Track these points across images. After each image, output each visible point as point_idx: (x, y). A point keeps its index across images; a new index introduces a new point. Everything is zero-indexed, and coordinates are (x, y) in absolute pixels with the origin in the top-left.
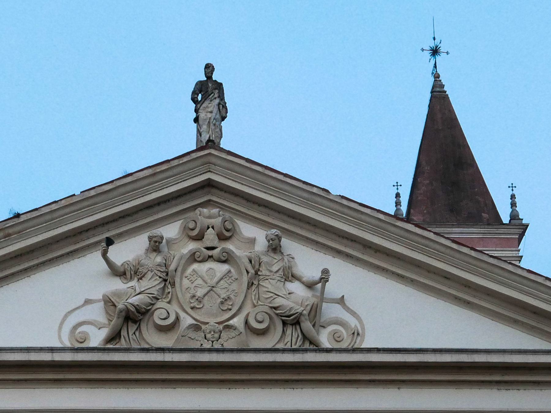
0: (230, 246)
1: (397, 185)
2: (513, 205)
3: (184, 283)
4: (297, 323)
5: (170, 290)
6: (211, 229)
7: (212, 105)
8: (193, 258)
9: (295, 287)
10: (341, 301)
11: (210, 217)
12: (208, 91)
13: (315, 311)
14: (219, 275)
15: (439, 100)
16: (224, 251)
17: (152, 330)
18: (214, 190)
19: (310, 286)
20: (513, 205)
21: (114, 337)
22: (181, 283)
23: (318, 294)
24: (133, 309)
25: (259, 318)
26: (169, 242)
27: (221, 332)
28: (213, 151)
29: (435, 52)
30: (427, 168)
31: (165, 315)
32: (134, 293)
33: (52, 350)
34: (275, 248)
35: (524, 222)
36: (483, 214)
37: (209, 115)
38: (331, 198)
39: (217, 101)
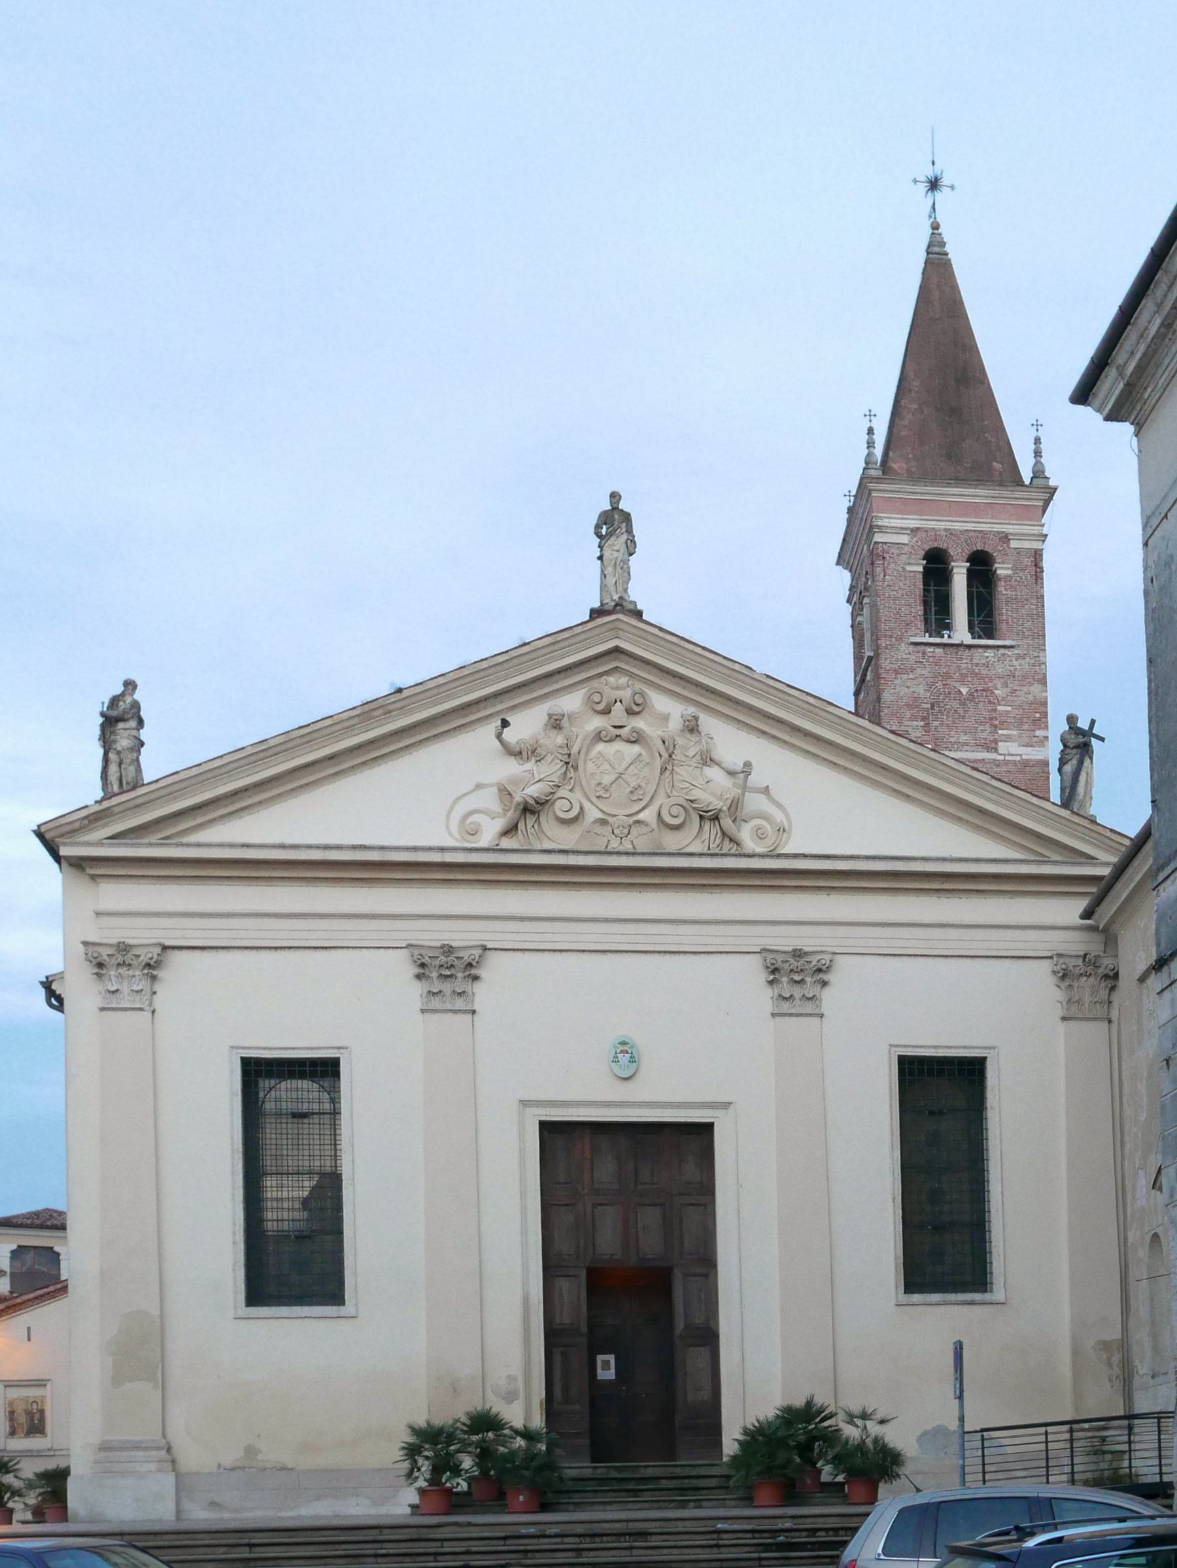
0: (639, 723)
1: (870, 415)
2: (1038, 454)
3: (589, 767)
4: (716, 818)
5: (572, 775)
6: (618, 703)
7: (619, 542)
8: (598, 737)
9: (713, 772)
10: (766, 791)
11: (618, 687)
12: (614, 523)
13: (735, 806)
14: (628, 759)
15: (938, 275)
16: (634, 730)
17: (552, 822)
18: (622, 657)
19: (731, 773)
20: (1038, 454)
21: (510, 830)
22: (585, 769)
23: (741, 782)
24: (532, 802)
25: (675, 811)
26: (571, 717)
27: (630, 826)
28: (620, 616)
29: (934, 184)
30: (916, 384)
31: (567, 806)
32: (534, 779)
33: (442, 849)
34: (692, 727)
35: (1052, 483)
36: (994, 464)
37: (615, 554)
38: (755, 676)
39: (625, 537)
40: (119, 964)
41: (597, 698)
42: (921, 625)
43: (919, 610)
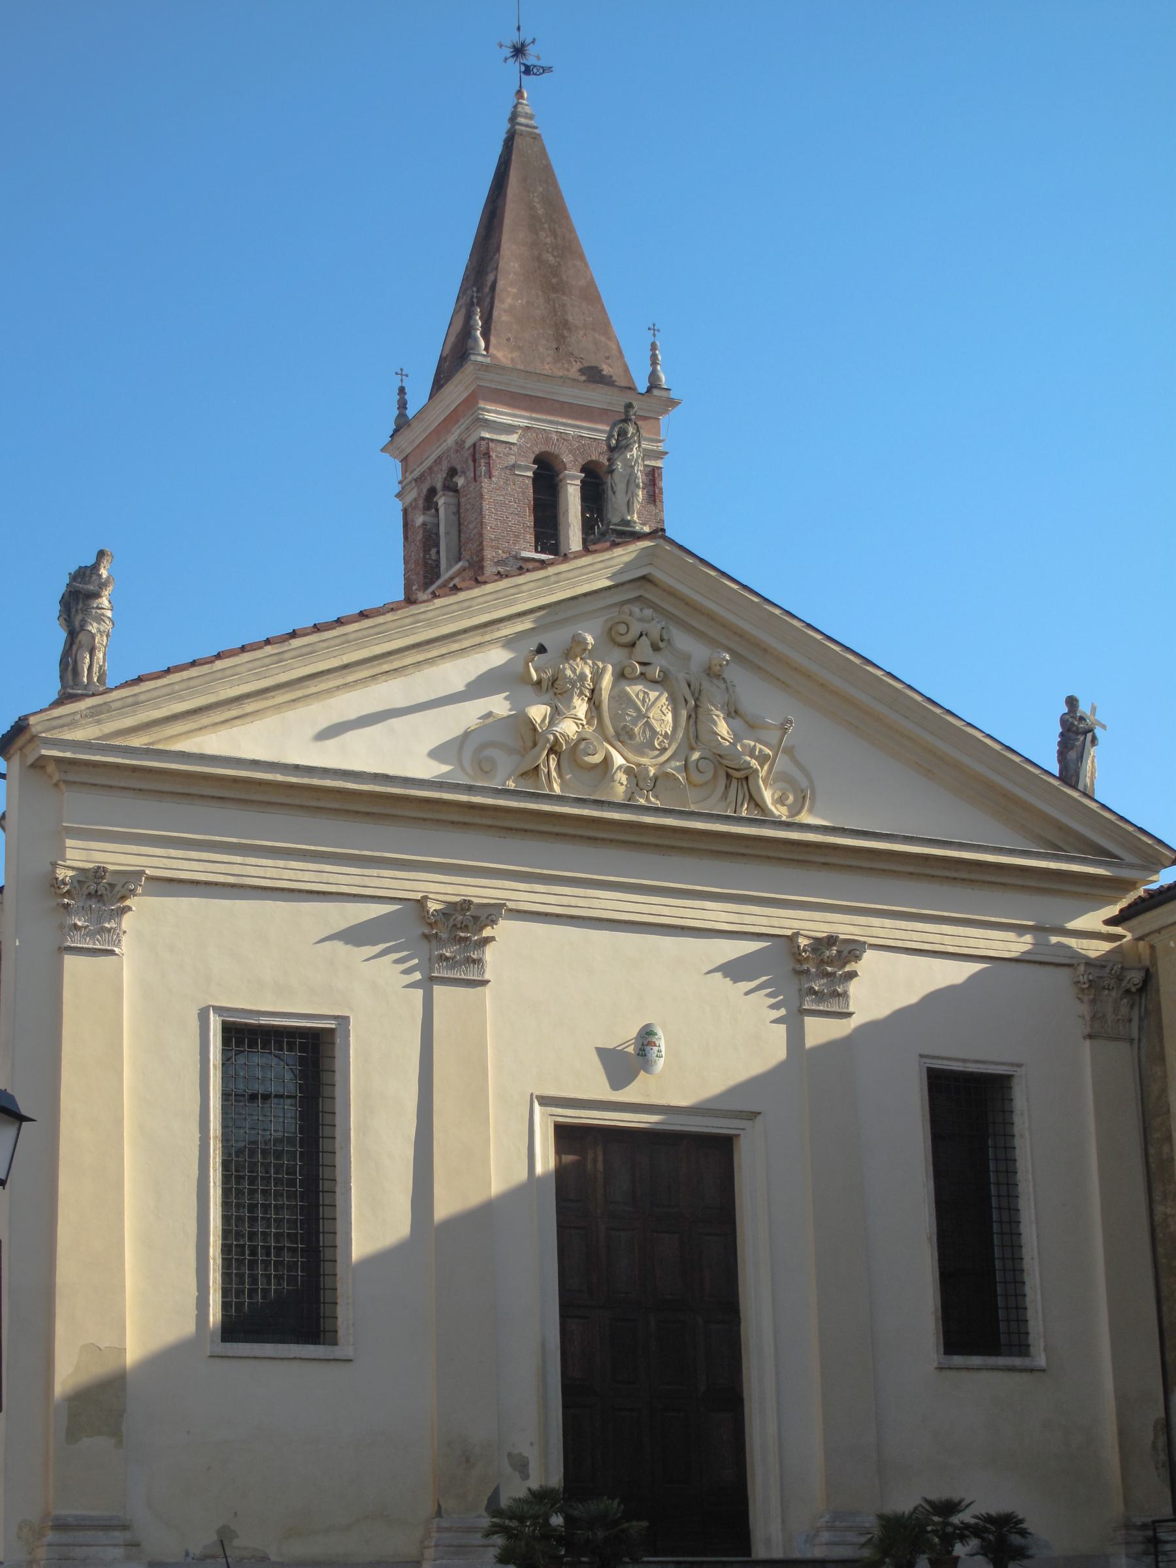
2: (654, 361)
20: (654, 361)
40: (89, 895)
41: (622, 629)
42: (530, 538)
43: (529, 520)
